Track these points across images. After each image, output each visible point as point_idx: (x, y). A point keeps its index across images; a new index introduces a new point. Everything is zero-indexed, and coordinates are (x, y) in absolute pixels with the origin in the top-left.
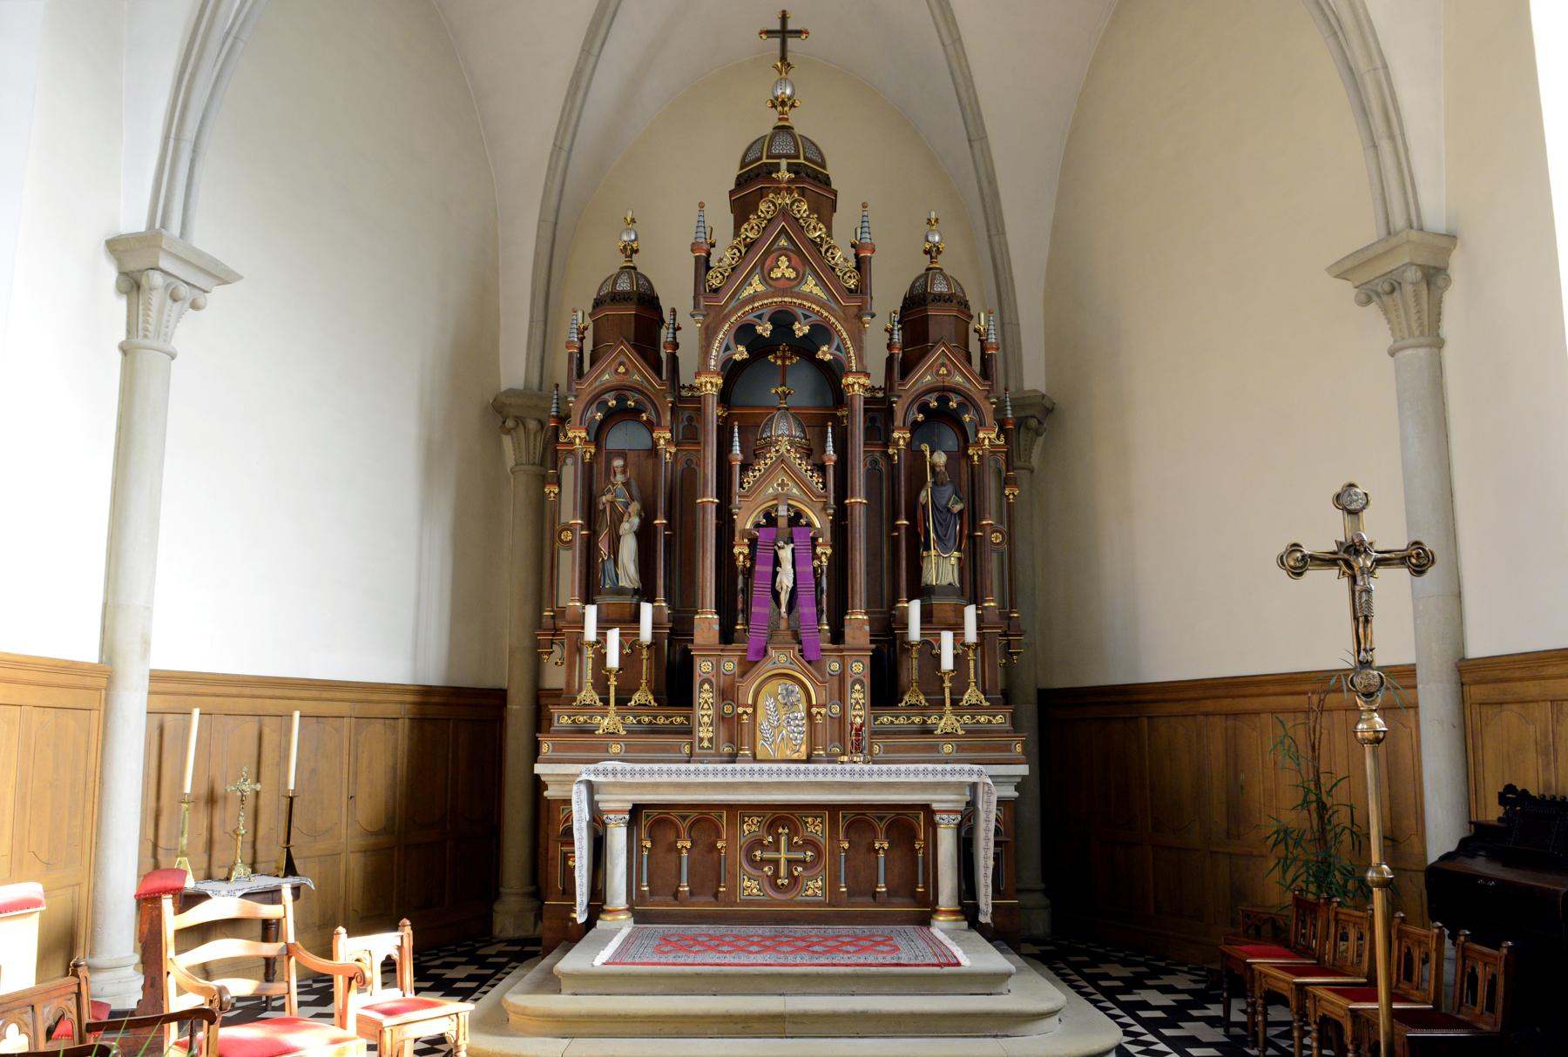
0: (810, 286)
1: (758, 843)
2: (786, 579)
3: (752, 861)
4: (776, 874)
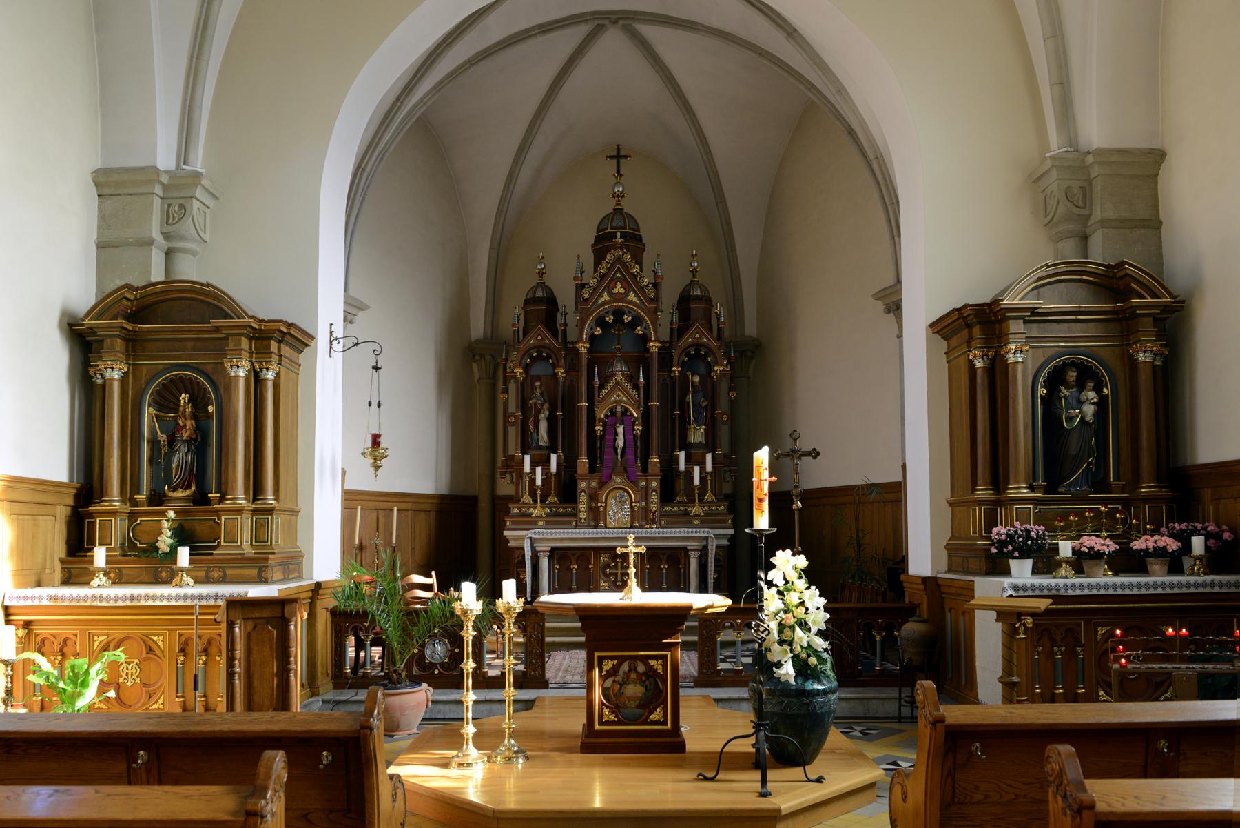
0: (632, 297)
1: (607, 566)
2: (620, 442)
3: (605, 574)
4: (616, 580)
